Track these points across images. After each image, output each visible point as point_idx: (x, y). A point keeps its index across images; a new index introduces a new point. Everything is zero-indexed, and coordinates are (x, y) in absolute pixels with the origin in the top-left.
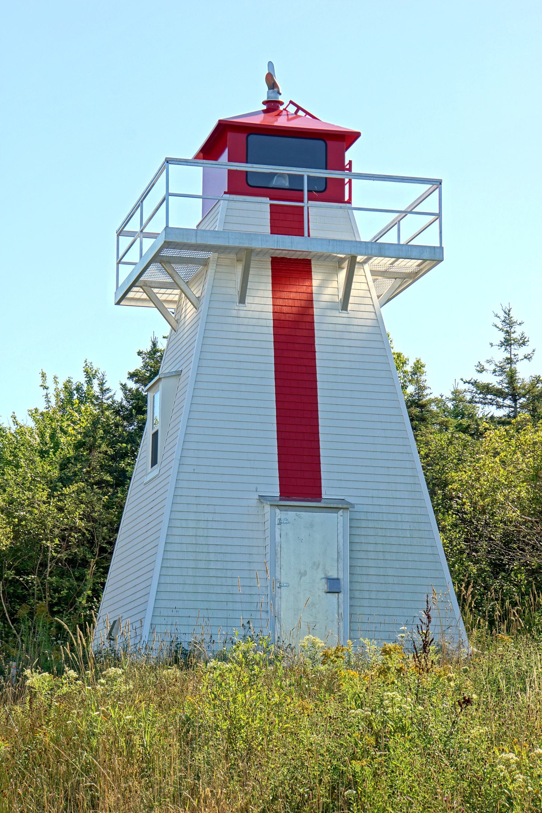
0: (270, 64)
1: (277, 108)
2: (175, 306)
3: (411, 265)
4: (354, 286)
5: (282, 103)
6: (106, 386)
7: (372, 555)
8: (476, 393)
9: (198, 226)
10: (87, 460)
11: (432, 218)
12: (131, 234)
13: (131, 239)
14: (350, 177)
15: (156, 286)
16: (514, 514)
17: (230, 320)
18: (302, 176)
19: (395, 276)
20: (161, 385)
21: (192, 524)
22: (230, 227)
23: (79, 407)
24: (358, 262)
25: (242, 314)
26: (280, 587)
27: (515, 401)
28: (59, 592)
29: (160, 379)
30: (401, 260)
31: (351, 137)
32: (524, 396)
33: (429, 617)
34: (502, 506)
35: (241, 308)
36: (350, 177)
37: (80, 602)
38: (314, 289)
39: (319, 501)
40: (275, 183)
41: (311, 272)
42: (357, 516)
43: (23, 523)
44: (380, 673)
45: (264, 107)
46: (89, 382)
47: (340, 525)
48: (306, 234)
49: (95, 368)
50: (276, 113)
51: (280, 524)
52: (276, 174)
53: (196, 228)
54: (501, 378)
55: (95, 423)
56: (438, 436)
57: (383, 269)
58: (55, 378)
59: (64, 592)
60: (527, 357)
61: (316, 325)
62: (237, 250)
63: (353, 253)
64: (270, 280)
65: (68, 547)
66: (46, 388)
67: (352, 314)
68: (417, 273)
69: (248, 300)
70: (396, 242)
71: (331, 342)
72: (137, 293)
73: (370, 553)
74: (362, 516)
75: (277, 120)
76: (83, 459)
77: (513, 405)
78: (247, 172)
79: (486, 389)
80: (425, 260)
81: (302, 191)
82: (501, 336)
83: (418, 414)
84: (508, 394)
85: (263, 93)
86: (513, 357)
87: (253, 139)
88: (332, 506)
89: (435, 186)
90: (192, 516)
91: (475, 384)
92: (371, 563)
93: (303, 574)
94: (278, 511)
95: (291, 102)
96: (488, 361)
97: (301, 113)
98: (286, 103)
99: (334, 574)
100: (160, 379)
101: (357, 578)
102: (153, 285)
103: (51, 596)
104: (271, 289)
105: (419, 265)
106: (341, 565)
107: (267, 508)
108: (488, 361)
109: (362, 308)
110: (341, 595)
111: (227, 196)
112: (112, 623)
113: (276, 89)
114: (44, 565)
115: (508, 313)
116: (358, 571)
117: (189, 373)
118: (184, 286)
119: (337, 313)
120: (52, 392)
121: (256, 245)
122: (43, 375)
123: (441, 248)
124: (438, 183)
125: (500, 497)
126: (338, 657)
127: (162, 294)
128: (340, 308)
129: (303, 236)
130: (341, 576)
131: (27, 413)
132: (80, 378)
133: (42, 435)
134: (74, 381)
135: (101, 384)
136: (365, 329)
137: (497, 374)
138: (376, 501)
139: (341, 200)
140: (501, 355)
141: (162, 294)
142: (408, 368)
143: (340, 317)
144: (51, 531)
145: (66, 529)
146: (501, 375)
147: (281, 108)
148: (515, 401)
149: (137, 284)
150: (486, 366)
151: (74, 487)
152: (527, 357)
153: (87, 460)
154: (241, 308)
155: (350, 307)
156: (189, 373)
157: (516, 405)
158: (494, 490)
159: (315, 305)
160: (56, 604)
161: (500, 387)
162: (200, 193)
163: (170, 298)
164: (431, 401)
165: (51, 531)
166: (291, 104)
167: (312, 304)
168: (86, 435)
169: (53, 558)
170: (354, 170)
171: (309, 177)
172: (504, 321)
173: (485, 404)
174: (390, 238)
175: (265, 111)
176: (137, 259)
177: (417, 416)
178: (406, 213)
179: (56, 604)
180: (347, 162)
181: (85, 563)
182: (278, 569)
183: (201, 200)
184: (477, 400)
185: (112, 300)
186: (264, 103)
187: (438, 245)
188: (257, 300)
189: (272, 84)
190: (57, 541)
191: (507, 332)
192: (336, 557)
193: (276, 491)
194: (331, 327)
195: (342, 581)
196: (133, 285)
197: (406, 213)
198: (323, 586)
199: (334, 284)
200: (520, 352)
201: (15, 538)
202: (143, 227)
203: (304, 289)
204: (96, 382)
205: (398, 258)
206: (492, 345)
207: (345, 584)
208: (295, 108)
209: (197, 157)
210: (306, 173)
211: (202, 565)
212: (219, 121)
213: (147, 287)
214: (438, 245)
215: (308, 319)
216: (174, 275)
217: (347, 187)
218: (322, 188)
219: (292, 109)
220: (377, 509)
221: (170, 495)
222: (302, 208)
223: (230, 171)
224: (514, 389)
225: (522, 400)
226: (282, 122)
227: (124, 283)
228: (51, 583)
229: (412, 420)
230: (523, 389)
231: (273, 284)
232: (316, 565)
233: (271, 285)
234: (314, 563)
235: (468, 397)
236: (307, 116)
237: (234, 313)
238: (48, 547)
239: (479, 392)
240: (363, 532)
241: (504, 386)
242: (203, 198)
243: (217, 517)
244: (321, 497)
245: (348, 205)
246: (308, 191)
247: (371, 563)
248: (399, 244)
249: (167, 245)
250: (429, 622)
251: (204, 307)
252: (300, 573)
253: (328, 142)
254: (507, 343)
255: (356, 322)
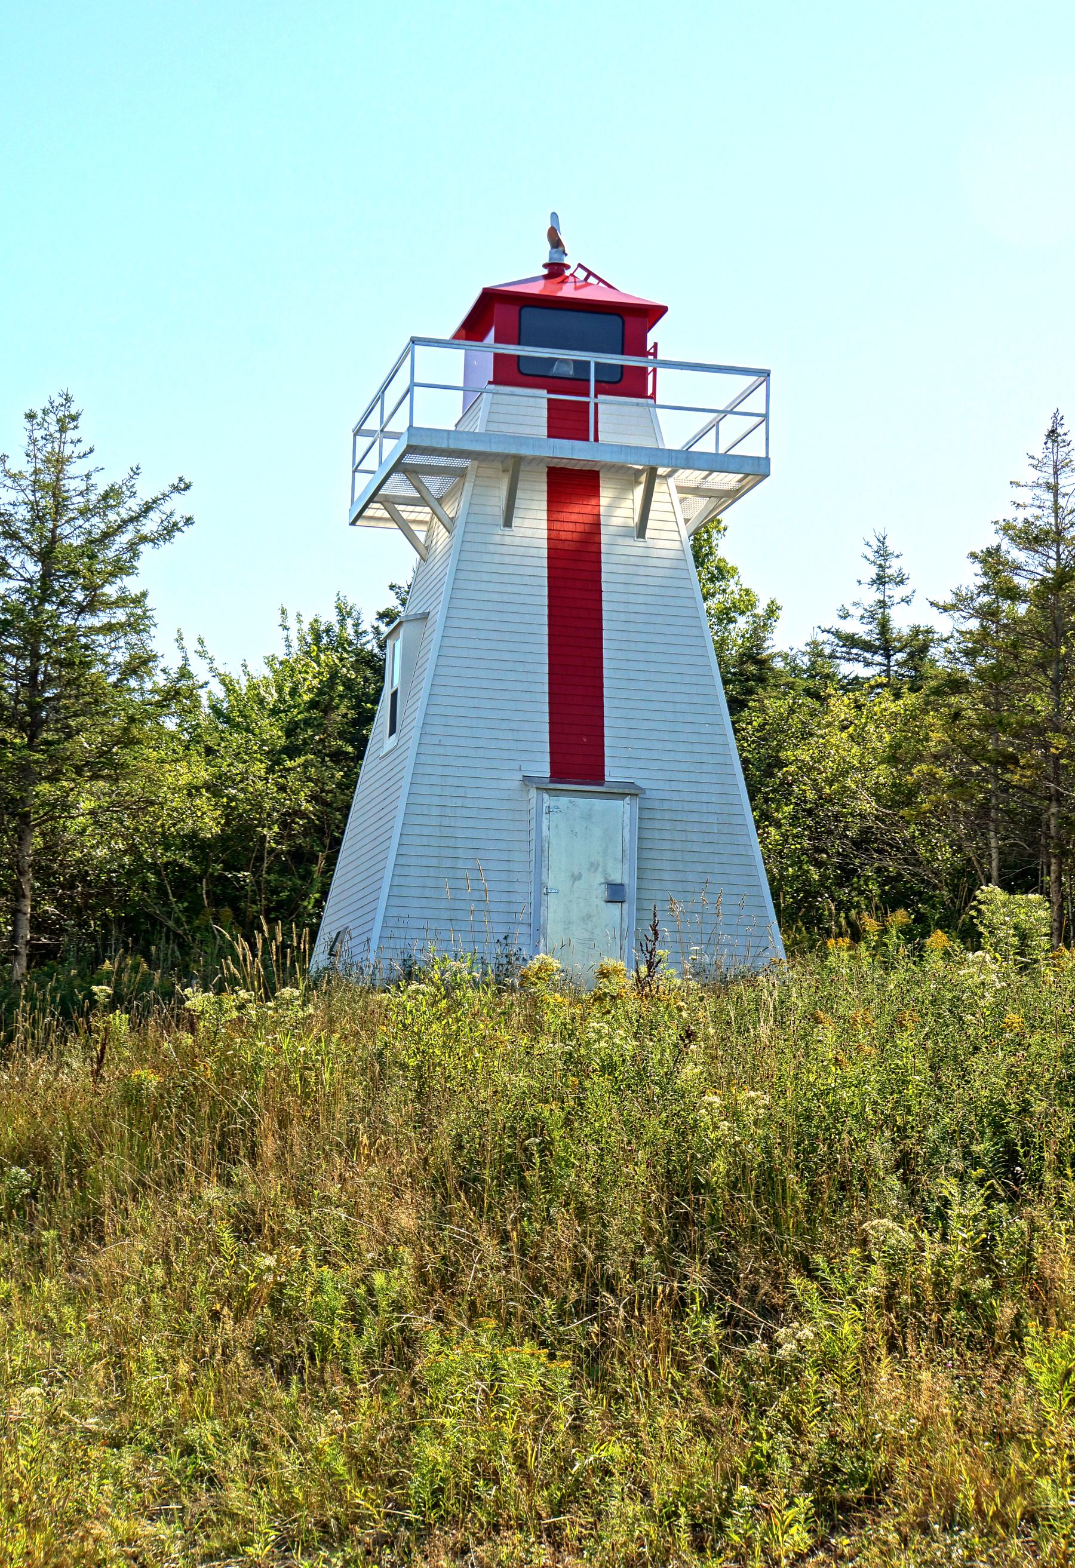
0: (554, 216)
1: (562, 273)
2: (425, 528)
3: (726, 481)
4: (654, 506)
5: (568, 267)
6: (361, 628)
7: (668, 855)
8: (837, 645)
9: (456, 425)
10: (321, 725)
11: (758, 419)
12: (370, 433)
13: (370, 440)
14: (655, 365)
15: (401, 501)
16: (866, 804)
17: (492, 548)
18: (588, 363)
19: (710, 494)
20: (402, 630)
21: (435, 811)
22: (493, 427)
23: (318, 656)
24: (661, 476)
25: (507, 540)
26: (547, 893)
27: (888, 657)
28: (278, 894)
29: (400, 624)
30: (715, 474)
31: (653, 313)
32: (900, 651)
33: (656, 934)
34: (854, 796)
35: (506, 533)
36: (655, 365)
37: (305, 907)
38: (602, 510)
39: (602, 785)
40: (555, 370)
41: (599, 487)
42: (648, 804)
43: (233, 804)
44: (595, 1000)
45: (545, 272)
46: (342, 622)
47: (627, 815)
48: (592, 438)
49: (350, 604)
50: (559, 279)
51: (548, 813)
52: (557, 359)
53: (453, 428)
54: (870, 627)
55: (334, 675)
56: (779, 703)
57: (693, 485)
58: (299, 615)
59: (284, 894)
60: (906, 600)
61: (603, 558)
62: (503, 458)
63: (653, 463)
64: (545, 497)
65: (291, 837)
66: (286, 628)
67: (650, 543)
68: (738, 491)
69: (515, 522)
70: (714, 451)
71: (622, 579)
72: (376, 510)
73: (445, 860)
74: (657, 805)
75: (561, 289)
76: (316, 723)
77: (886, 662)
78: (518, 356)
79: (851, 641)
80: (747, 475)
81: (588, 380)
82: (873, 572)
83: (755, 672)
84: (879, 648)
85: (544, 253)
86: (887, 599)
87: (527, 312)
88: (616, 791)
89: (762, 379)
90: (436, 801)
91: (837, 634)
92: (666, 865)
93: (576, 878)
94: (546, 796)
95: (580, 265)
96: (855, 604)
97: (592, 280)
98: (573, 267)
99: (616, 878)
100: (400, 624)
101: (646, 884)
102: (397, 500)
103: (266, 899)
104: (546, 508)
105: (740, 481)
106: (626, 866)
107: (533, 793)
108: (855, 604)
109: (664, 535)
110: (625, 906)
111: (492, 387)
112: (334, 936)
113: (560, 249)
114: (260, 859)
115: (882, 541)
116: (648, 875)
117: (438, 616)
118: (435, 504)
119: (629, 541)
120: (293, 635)
121: (525, 451)
122: (283, 612)
123: (767, 459)
124: (766, 374)
125: (849, 783)
126: (539, 978)
127: (408, 513)
128: (635, 534)
129: (588, 440)
130: (626, 881)
131: (262, 660)
132: (330, 617)
133: (280, 689)
134: (323, 620)
135: (356, 625)
136: (667, 563)
137: (865, 621)
138: (675, 786)
139: (641, 393)
140: (871, 596)
141: (408, 513)
142: (760, 610)
143: (635, 547)
144: (269, 815)
145: (289, 815)
146: (870, 623)
147: (567, 273)
148: (888, 657)
149: (376, 499)
150: (852, 610)
151: (300, 760)
152: (906, 600)
153: (321, 725)
154: (506, 533)
155: (648, 533)
156: (438, 616)
157: (889, 662)
158: (844, 774)
159: (603, 530)
160: (274, 909)
161: (868, 638)
162: (461, 384)
163: (421, 517)
164: (772, 656)
165: (269, 815)
166: (579, 269)
167: (599, 529)
168: (321, 692)
169: (273, 850)
170: (660, 357)
171: (597, 364)
172: (877, 552)
173: (849, 660)
174: (706, 446)
175: (545, 277)
176: (375, 467)
177: (754, 675)
178: (725, 413)
179: (274, 909)
180: (649, 345)
181: (314, 859)
182: (544, 870)
183: (461, 392)
184: (838, 655)
185: (347, 519)
186: (545, 266)
187: (764, 455)
188: (527, 523)
189: (555, 240)
190: (276, 829)
191: (880, 566)
192: (620, 857)
193: (544, 770)
194: (623, 560)
195: (627, 887)
196: (371, 500)
197: (725, 413)
198: (602, 893)
199: (628, 503)
200: (896, 592)
201: (227, 823)
202: (384, 424)
203: (588, 509)
204: (350, 622)
205: (712, 472)
206: (859, 582)
207: (631, 891)
208: (586, 274)
209: (457, 336)
210: (593, 358)
211: (448, 863)
212: (485, 290)
213: (389, 503)
214: (764, 455)
215: (594, 549)
216: (422, 488)
217: (650, 378)
218: (617, 379)
219: (581, 274)
220: (675, 796)
221: (407, 774)
222: (588, 403)
223: (496, 355)
224: (887, 641)
225: (900, 656)
226: (567, 291)
227: (360, 498)
228: (268, 882)
229: (726, 682)
230: (899, 640)
231: (549, 501)
232: (593, 867)
233: (546, 503)
234: (592, 864)
235: (827, 651)
236: (601, 284)
237: (497, 539)
238: (265, 836)
239: (841, 644)
240: (657, 825)
241: (874, 638)
242: (464, 389)
243: (468, 803)
244: (604, 779)
245: (651, 401)
246: (596, 381)
247: (666, 865)
248: (717, 454)
249: (411, 449)
250: (656, 939)
251: (458, 531)
252: (573, 875)
253: (626, 319)
254: (880, 580)
255: (655, 553)
